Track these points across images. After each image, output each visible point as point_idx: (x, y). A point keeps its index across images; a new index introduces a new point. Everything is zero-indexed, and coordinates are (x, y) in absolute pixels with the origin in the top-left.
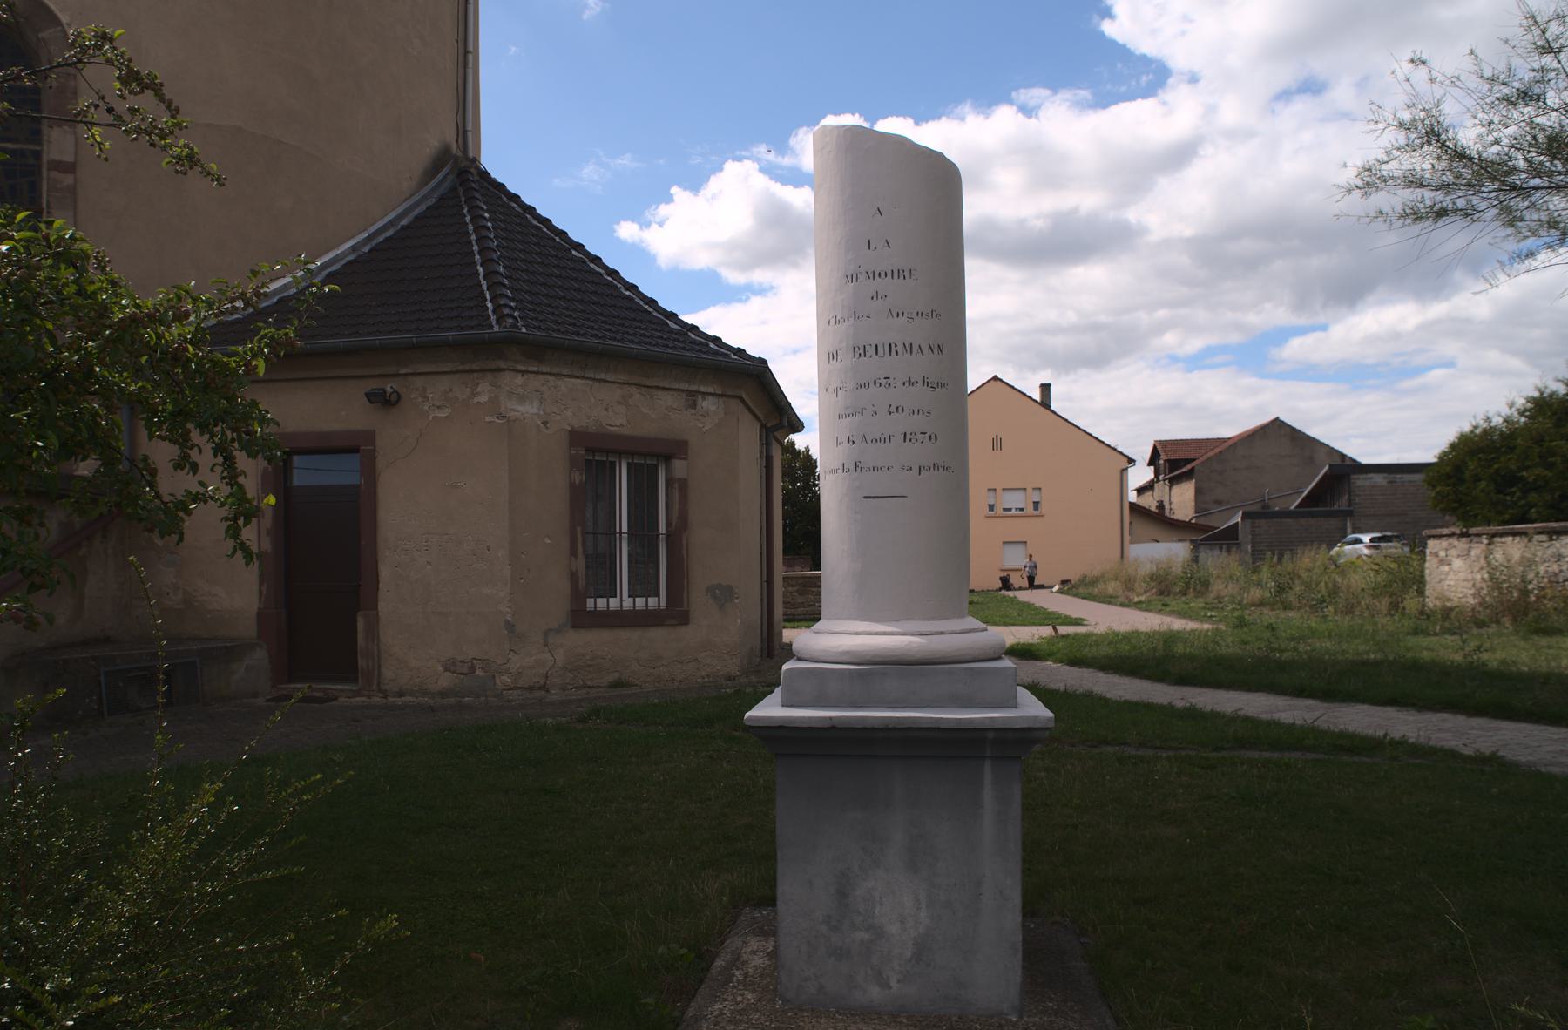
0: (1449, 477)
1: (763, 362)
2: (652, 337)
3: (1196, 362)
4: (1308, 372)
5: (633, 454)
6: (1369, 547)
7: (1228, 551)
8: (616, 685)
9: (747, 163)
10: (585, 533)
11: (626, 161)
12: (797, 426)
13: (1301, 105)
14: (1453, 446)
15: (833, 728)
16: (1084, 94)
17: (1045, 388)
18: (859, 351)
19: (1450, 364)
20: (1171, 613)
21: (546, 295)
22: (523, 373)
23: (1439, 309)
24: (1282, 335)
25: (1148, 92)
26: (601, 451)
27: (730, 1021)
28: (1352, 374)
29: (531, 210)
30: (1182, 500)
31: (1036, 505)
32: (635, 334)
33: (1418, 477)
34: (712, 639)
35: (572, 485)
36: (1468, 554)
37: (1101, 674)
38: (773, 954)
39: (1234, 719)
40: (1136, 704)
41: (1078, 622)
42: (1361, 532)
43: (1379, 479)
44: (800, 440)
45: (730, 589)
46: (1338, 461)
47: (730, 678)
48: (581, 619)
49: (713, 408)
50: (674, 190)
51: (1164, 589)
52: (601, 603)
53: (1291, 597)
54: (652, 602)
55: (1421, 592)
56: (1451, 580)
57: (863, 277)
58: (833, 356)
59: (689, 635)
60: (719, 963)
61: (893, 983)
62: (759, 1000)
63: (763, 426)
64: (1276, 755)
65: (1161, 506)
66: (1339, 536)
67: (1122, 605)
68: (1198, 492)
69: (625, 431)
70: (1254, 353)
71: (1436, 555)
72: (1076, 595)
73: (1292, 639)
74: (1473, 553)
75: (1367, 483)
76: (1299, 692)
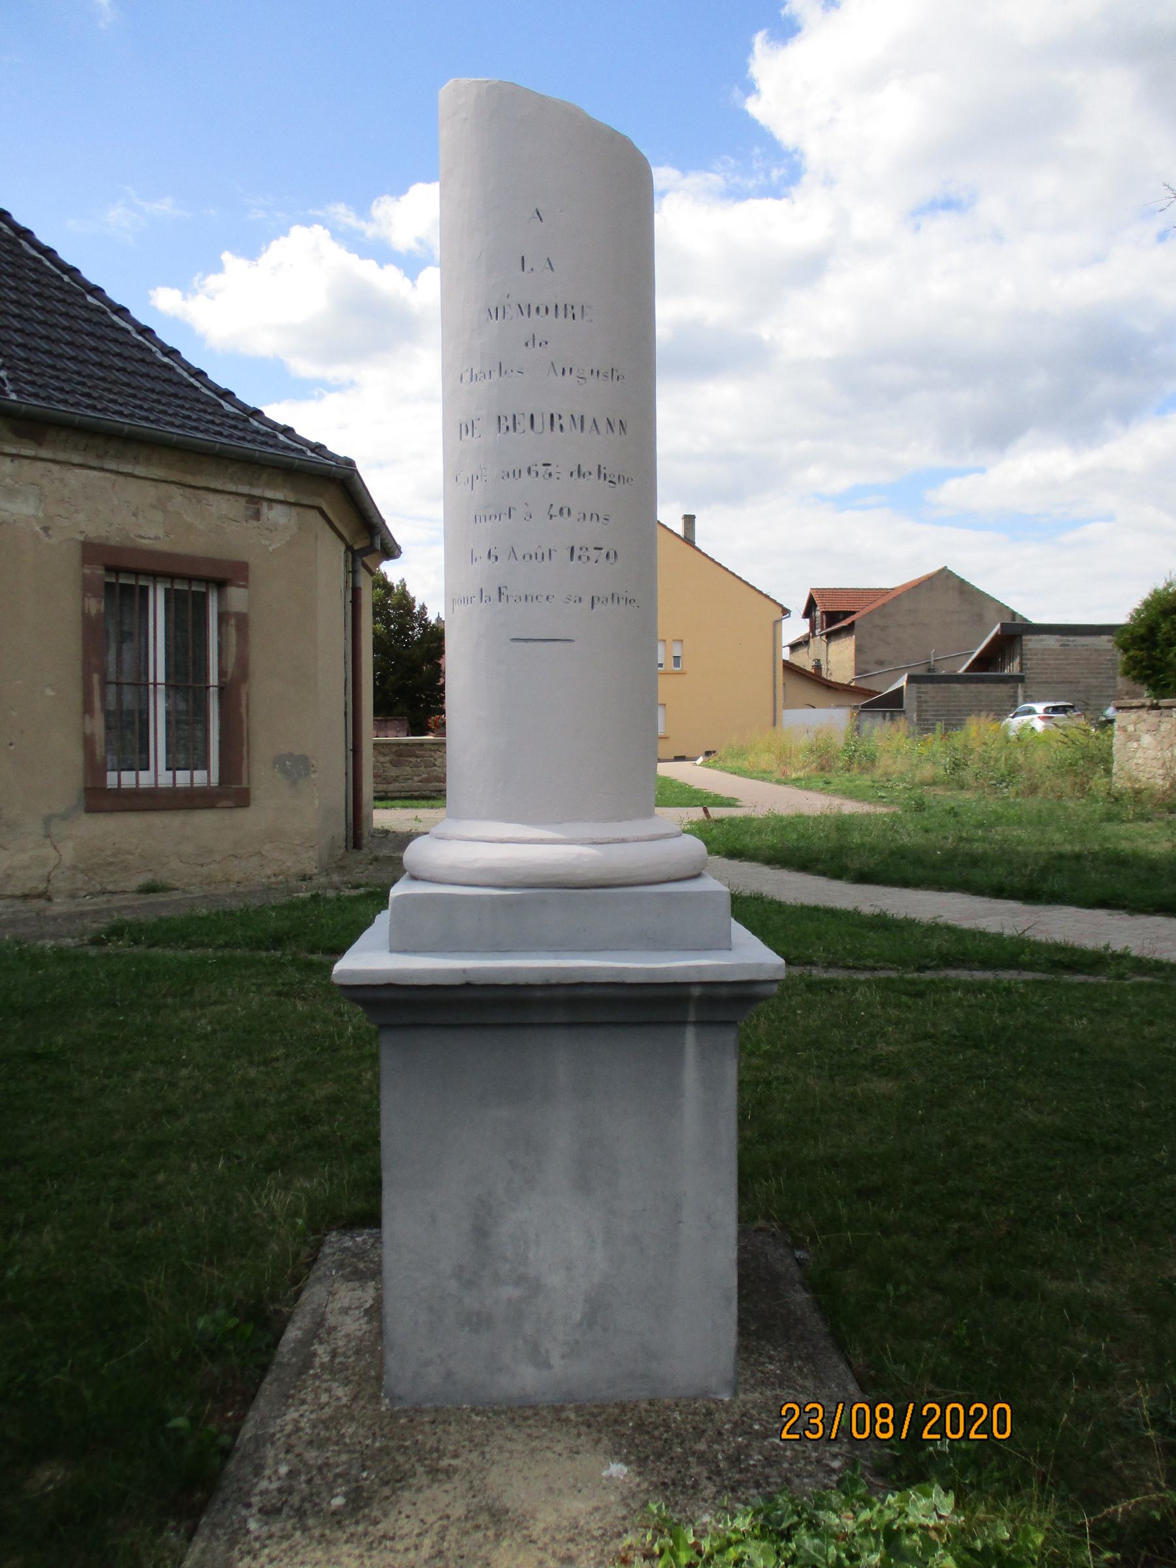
0: (1143, 639)
1: (350, 463)
2: (198, 420)
3: (847, 500)
4: (968, 519)
5: (172, 577)
6: (1042, 718)
7: (892, 719)
8: (149, 889)
9: (318, 229)
10: (105, 682)
11: (165, 207)
12: (390, 551)
13: (943, 225)
14: (1147, 605)
15: (468, 986)
16: (715, 180)
17: (689, 520)
18: (507, 423)
19: (1109, 518)
20: (836, 792)
21: (48, 353)
22: (14, 457)
23: (1093, 458)
24: (936, 477)
25: (774, 192)
26: (129, 571)
27: (310, 1443)
28: (1015, 525)
29: (26, 234)
30: (840, 659)
31: (677, 659)
32: (175, 415)
33: (1104, 641)
34: (277, 835)
35: (85, 616)
36: (1157, 729)
37: (766, 869)
38: (375, 1312)
39: (934, 929)
40: (816, 909)
41: (730, 803)
42: (1033, 701)
43: (1051, 641)
44: (391, 571)
45: (304, 759)
46: (1008, 621)
47: (305, 878)
48: (99, 799)
49: (283, 521)
50: (226, 257)
51: (824, 766)
52: (128, 779)
53: (967, 775)
54: (200, 777)
55: (1108, 772)
56: (1139, 758)
57: (513, 311)
58: (467, 428)
59: (248, 821)
60: (293, 1333)
61: (556, 1360)
62: (355, 1398)
63: (349, 548)
64: (988, 975)
65: (818, 667)
66: (1009, 707)
67: (778, 782)
68: (859, 650)
69: (163, 546)
70: (908, 495)
71: (1124, 729)
72: (723, 769)
73: (980, 825)
74: (1162, 728)
75: (1039, 646)
76: (999, 892)
